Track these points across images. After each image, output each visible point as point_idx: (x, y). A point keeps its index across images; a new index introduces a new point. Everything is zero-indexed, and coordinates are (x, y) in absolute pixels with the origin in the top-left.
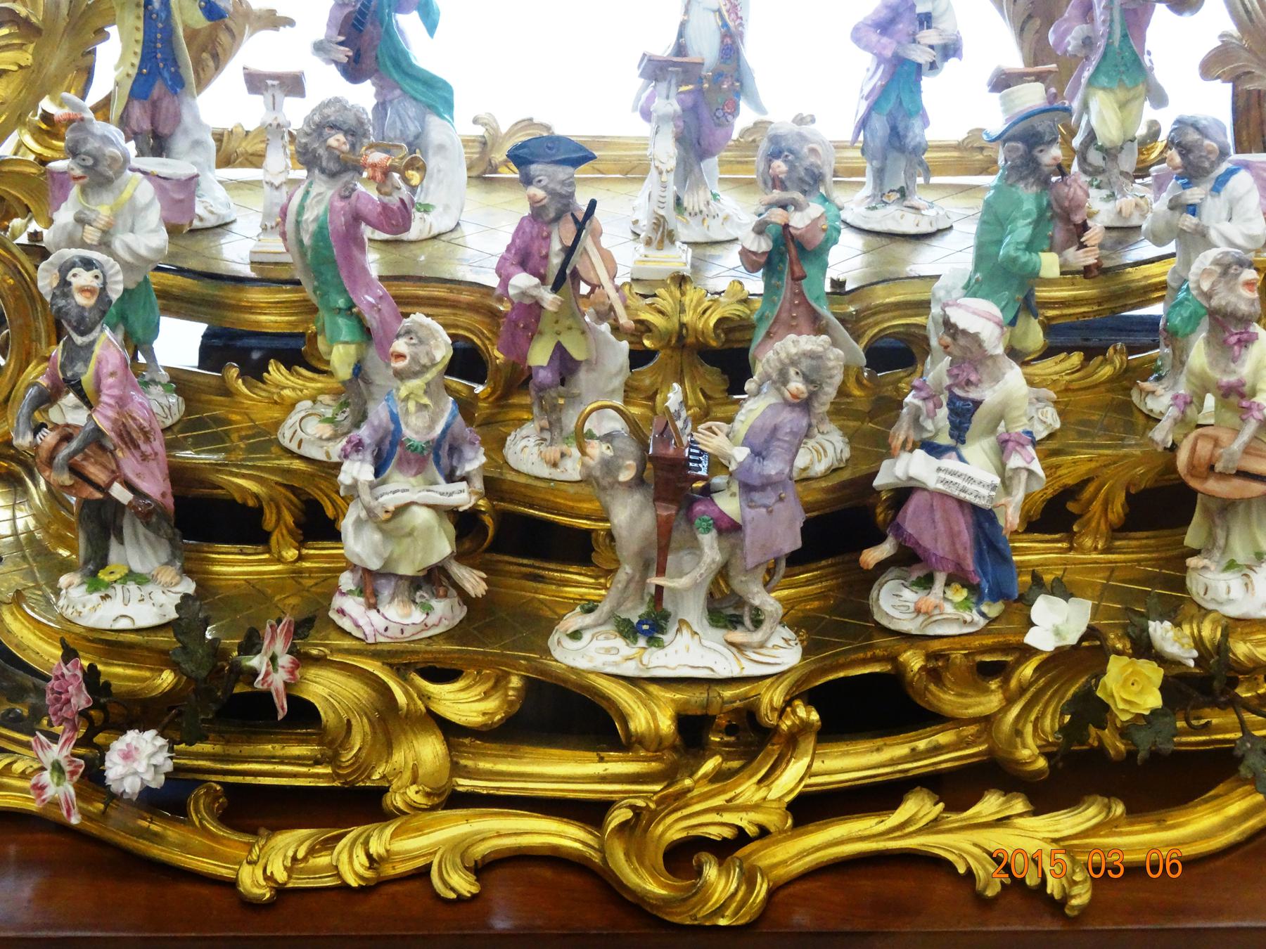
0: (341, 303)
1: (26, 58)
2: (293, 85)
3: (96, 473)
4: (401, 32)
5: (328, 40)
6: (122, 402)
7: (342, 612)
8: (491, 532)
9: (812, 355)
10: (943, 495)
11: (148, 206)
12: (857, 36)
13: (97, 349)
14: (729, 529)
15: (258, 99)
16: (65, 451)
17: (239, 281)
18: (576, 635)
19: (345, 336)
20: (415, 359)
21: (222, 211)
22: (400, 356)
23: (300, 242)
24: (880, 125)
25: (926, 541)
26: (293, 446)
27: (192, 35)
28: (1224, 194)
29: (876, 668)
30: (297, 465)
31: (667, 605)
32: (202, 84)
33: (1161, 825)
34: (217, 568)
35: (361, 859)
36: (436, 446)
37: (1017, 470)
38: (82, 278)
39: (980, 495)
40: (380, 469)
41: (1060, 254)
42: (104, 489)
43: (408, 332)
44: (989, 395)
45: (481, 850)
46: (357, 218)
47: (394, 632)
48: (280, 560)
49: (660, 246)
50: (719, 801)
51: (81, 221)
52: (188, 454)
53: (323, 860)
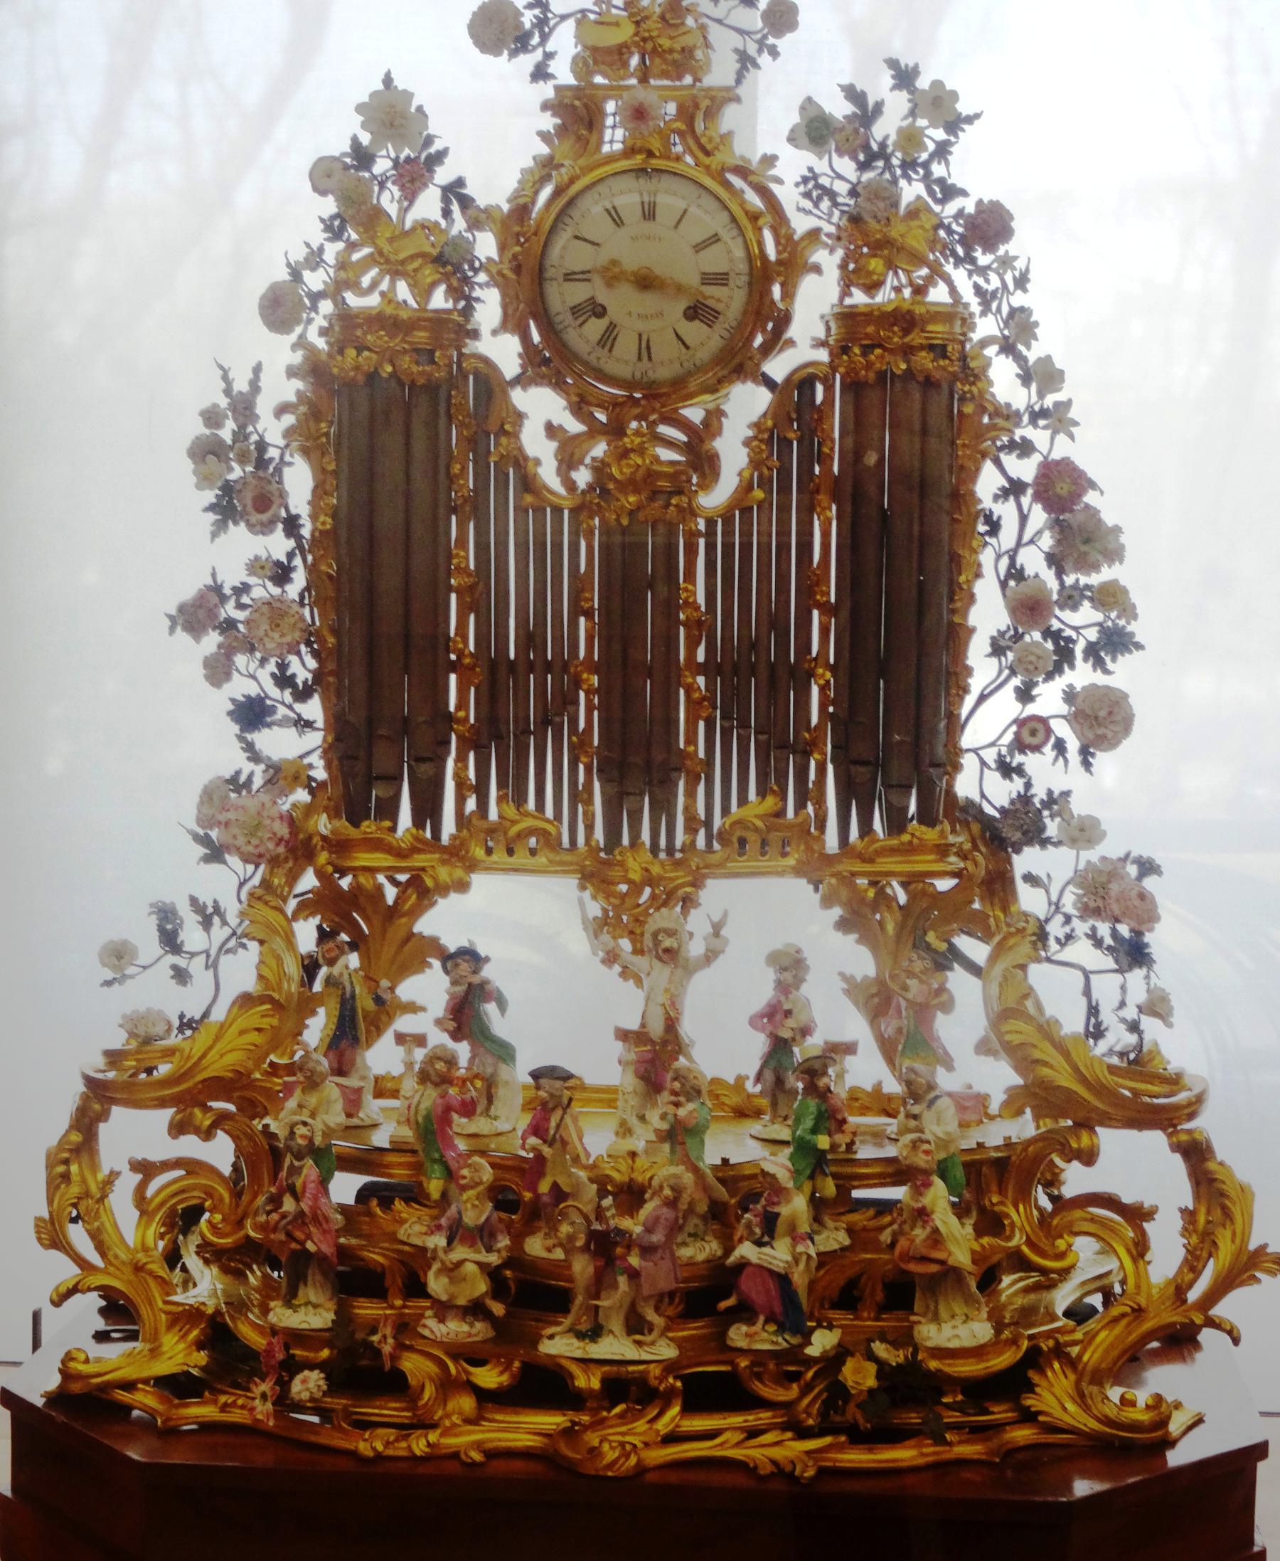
0: (437, 1156)
1: (275, 1022)
2: (420, 1040)
3: (299, 1235)
4: (486, 1014)
5: (444, 1018)
6: (316, 1199)
7: (425, 1326)
8: (513, 1291)
9: (675, 1176)
10: (760, 1267)
11: (336, 1100)
12: (754, 1022)
13: (305, 1171)
14: (634, 1275)
15: (401, 1049)
16: (284, 1222)
17: (381, 1150)
18: (551, 1337)
19: (438, 1175)
20: (472, 1179)
21: (375, 1117)
22: (464, 1177)
23: (417, 1122)
24: (769, 1075)
25: (754, 1295)
26: (405, 1239)
27: (366, 1015)
28: (934, 1108)
29: (723, 1368)
30: (407, 1248)
31: (601, 1319)
32: (369, 1045)
33: (870, 1451)
34: (357, 1311)
35: (423, 1443)
36: (481, 1229)
37: (801, 1254)
38: (301, 1130)
39: (779, 1266)
40: (450, 1241)
41: (830, 1136)
42: (302, 1243)
43: (469, 1166)
44: (784, 1210)
45: (491, 1445)
46: (448, 1109)
47: (452, 1336)
48: (392, 1307)
49: (624, 1136)
50: (623, 1429)
51: (300, 1106)
52: (342, 1240)
53: (404, 1444)
